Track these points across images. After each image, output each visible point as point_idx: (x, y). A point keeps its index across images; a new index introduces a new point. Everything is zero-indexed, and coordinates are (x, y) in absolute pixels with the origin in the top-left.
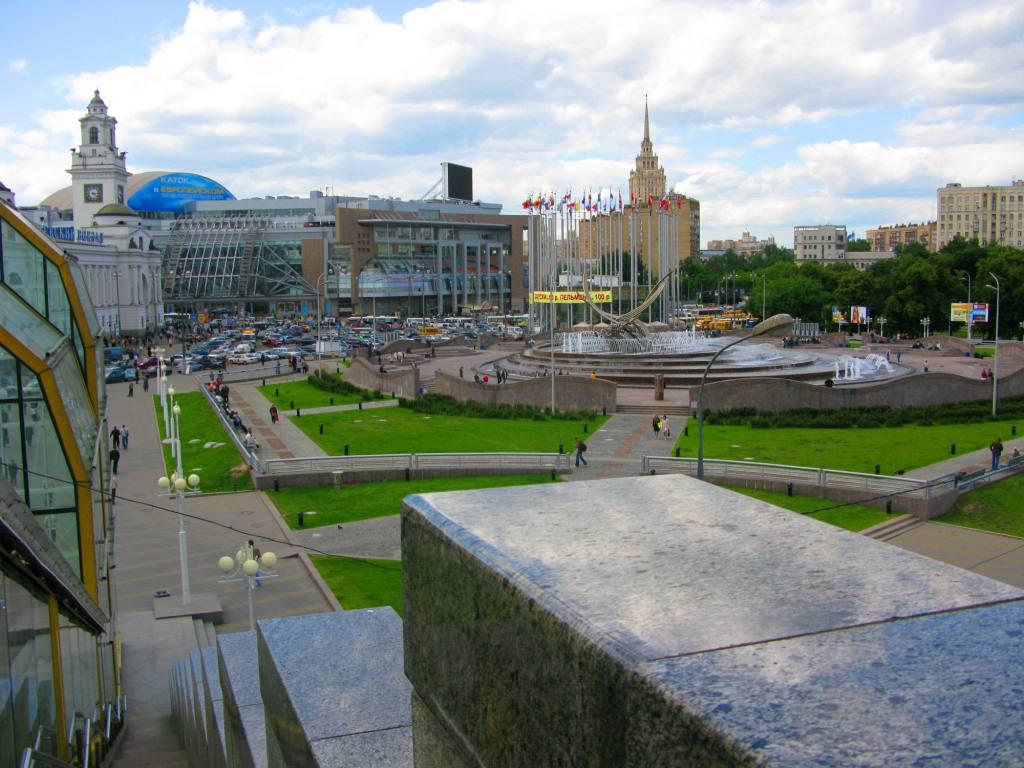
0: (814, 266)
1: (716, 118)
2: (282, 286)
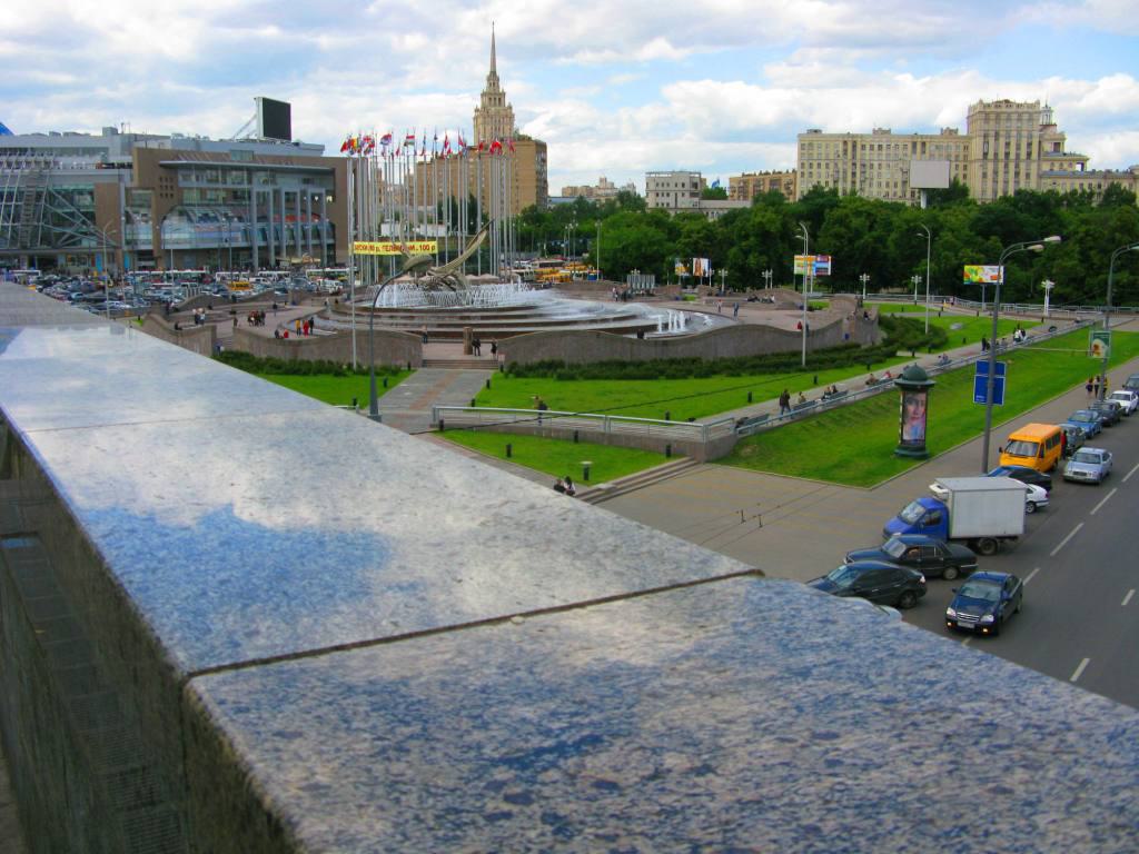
0: (661, 215)
1: (569, 52)
2: (72, 237)
